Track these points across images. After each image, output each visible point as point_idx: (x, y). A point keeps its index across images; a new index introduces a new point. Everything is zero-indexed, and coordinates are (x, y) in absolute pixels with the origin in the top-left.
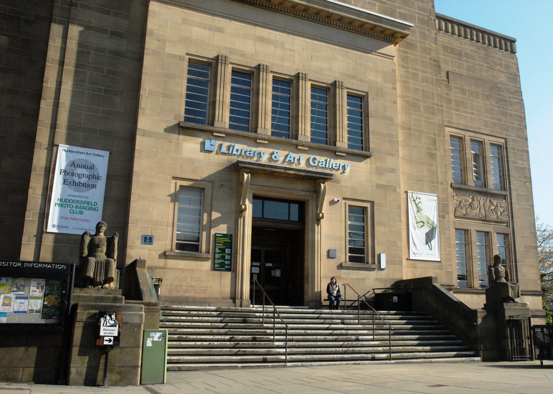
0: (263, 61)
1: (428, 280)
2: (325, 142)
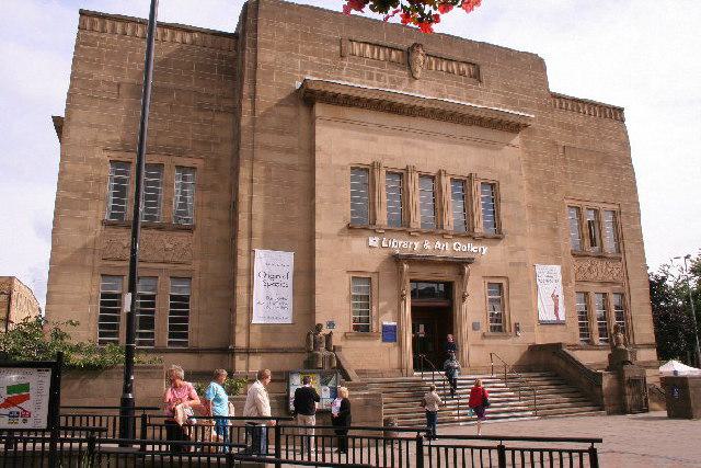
0: (411, 163)
1: (558, 346)
2: (469, 234)
